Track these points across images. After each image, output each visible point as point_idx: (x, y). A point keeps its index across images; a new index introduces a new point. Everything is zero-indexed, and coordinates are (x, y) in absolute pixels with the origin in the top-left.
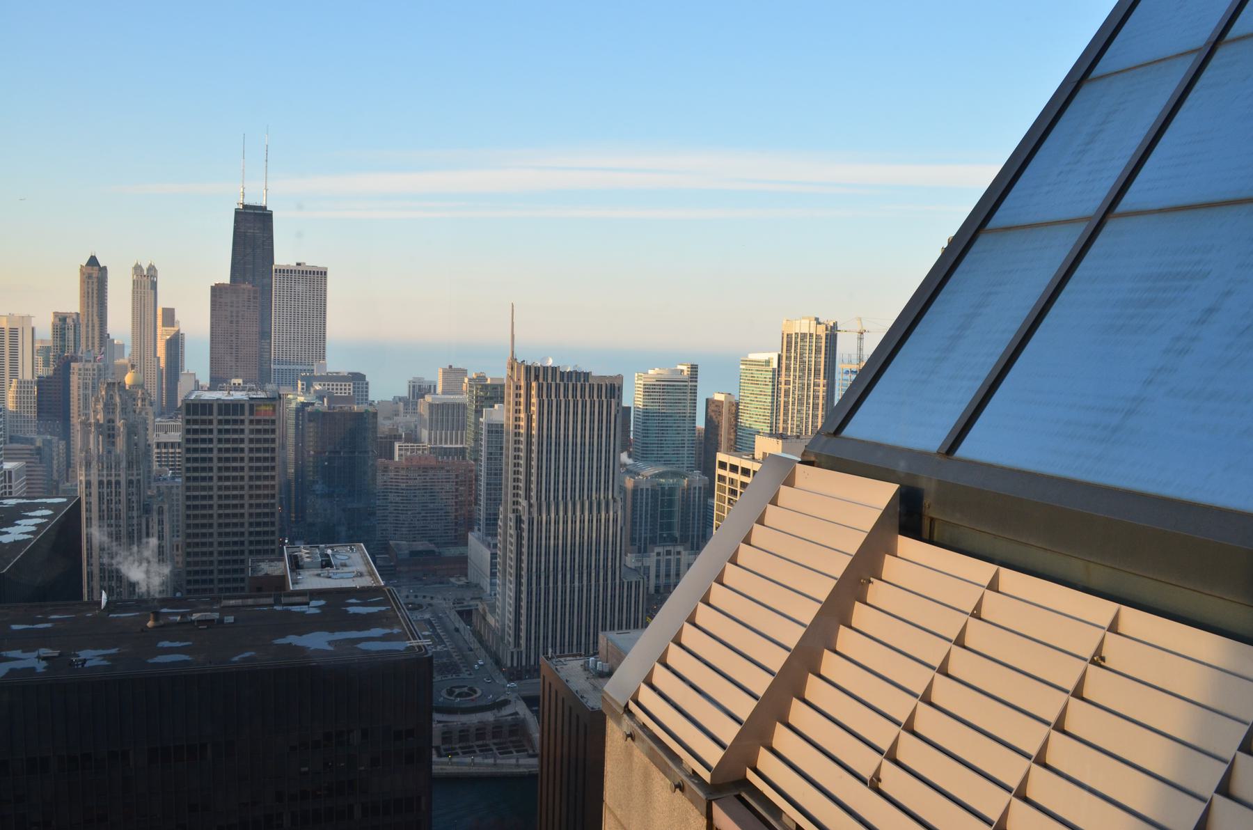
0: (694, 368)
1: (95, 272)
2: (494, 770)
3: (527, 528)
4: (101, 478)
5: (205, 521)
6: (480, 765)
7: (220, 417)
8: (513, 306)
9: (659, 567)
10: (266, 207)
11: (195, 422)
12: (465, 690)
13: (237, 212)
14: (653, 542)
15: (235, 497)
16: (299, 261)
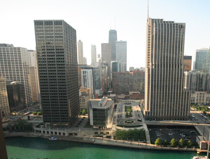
2: (130, 146)
6: (126, 143)
8: (199, 139)
12: (131, 121)
14: (196, 90)
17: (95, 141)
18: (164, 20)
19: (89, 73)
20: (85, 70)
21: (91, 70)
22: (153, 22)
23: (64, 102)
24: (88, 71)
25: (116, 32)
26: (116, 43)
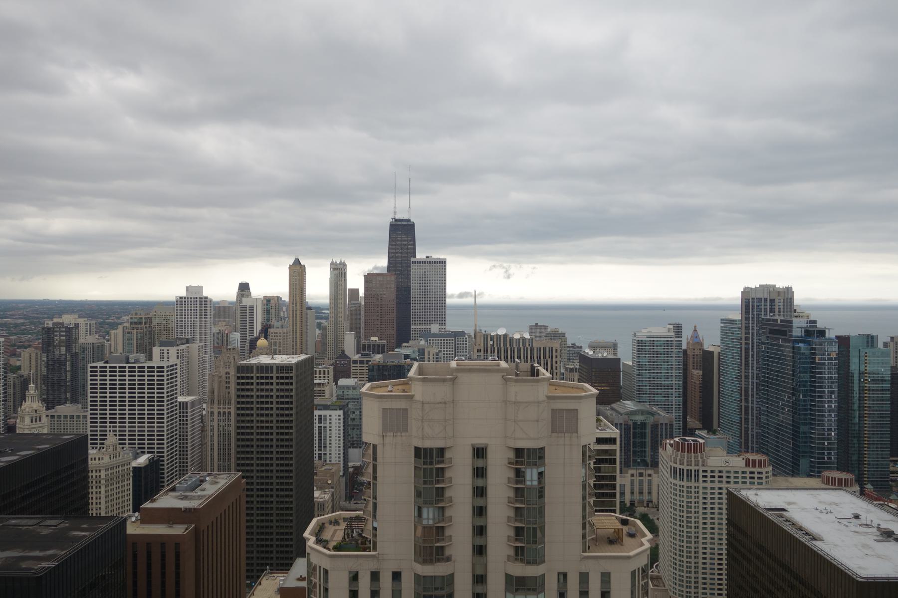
1: (298, 267)
4: (219, 410)
7: (258, 375)
9: (633, 486)
10: (410, 220)
11: (243, 378)
13: (391, 225)
15: (267, 427)
16: (428, 255)
19: (333, 421)
20: (322, 413)
21: (341, 412)
23: (287, 421)
25: (413, 225)
26: (413, 266)
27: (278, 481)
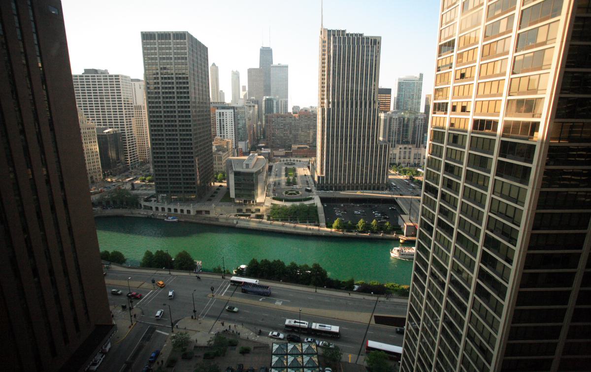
0: (421, 75)
3: (500, 339)
5: (172, 110)
6: (287, 227)
12: (294, 192)
14: (398, 142)
17: (237, 223)
18: (347, 32)
19: (228, 116)
20: (222, 111)
21: (232, 111)
22: (329, 36)
24: (226, 113)
27: (180, 124)
